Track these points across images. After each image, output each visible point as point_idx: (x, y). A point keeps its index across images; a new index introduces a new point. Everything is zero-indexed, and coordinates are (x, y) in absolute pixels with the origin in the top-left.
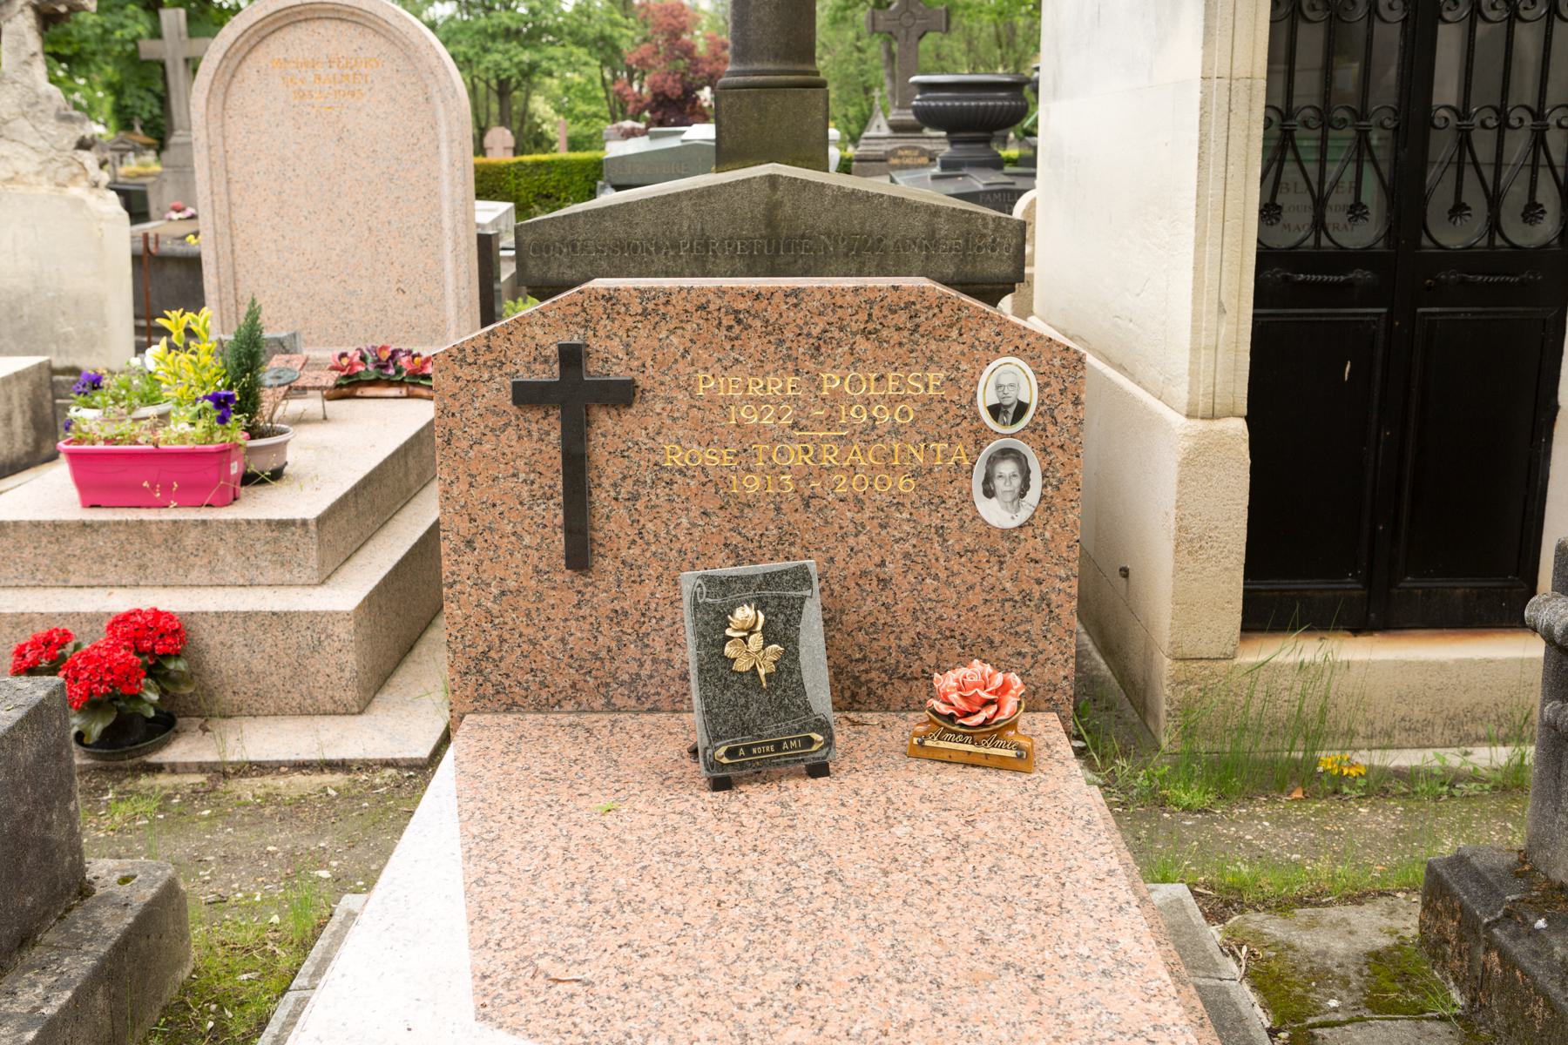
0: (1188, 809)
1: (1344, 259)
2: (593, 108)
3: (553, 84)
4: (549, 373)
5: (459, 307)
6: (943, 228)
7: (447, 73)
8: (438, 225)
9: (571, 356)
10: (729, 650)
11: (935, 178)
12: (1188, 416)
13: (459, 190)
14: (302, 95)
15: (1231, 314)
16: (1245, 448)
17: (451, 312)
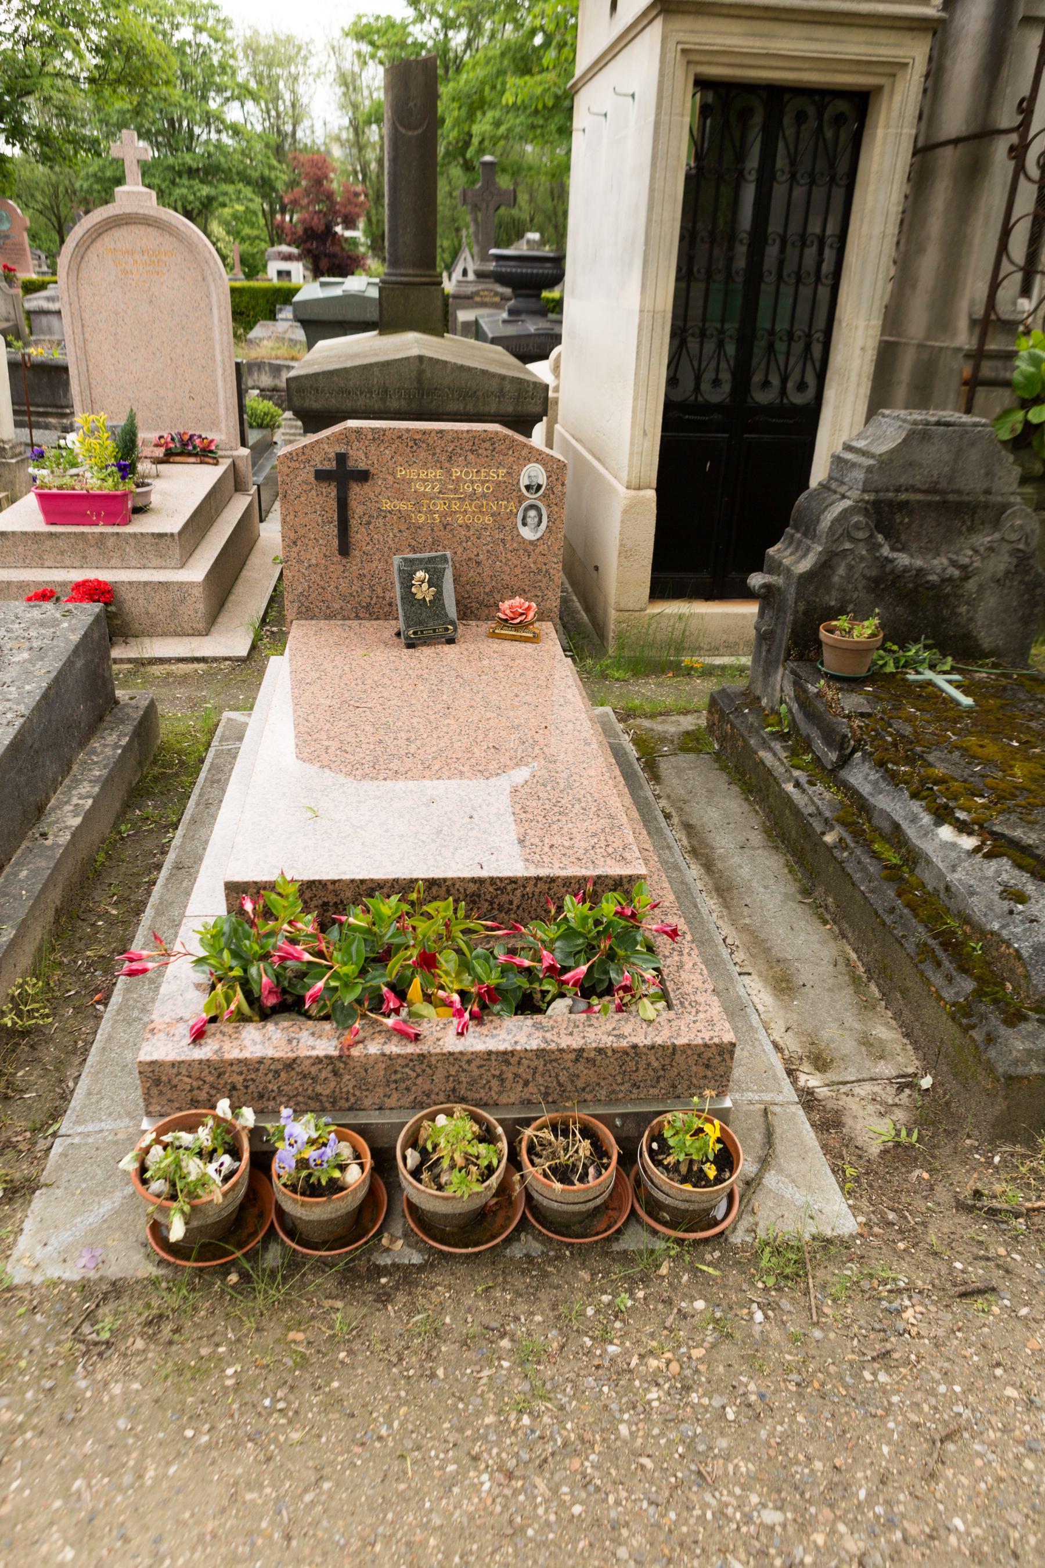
0: (617, 680)
1: (708, 408)
2: (255, 232)
3: (227, 212)
4: (332, 466)
5: (227, 409)
6: (507, 386)
7: (216, 263)
8: (213, 358)
9: (341, 458)
10: (413, 590)
11: (504, 322)
12: (628, 488)
13: (225, 337)
14: (125, 272)
15: (649, 436)
16: (654, 505)
17: (222, 411)
